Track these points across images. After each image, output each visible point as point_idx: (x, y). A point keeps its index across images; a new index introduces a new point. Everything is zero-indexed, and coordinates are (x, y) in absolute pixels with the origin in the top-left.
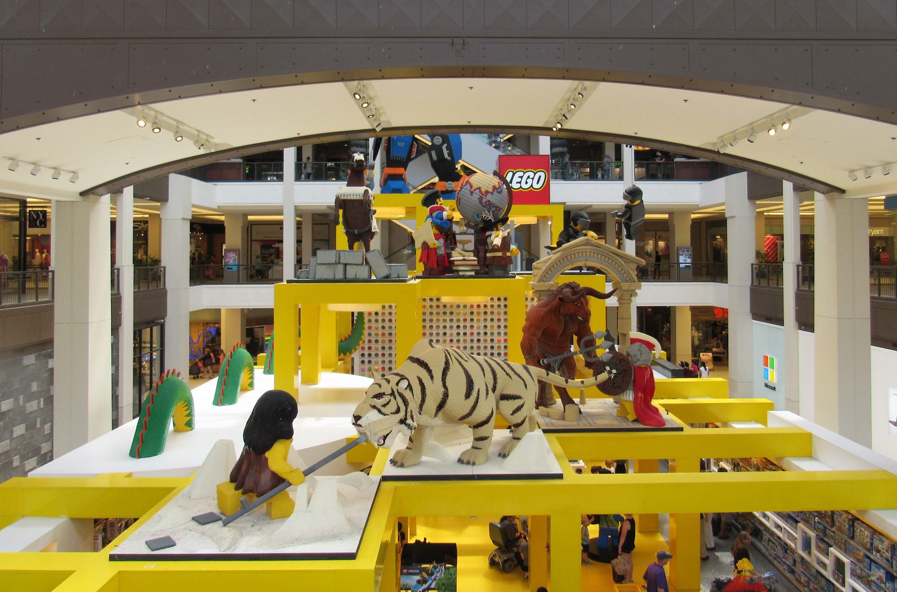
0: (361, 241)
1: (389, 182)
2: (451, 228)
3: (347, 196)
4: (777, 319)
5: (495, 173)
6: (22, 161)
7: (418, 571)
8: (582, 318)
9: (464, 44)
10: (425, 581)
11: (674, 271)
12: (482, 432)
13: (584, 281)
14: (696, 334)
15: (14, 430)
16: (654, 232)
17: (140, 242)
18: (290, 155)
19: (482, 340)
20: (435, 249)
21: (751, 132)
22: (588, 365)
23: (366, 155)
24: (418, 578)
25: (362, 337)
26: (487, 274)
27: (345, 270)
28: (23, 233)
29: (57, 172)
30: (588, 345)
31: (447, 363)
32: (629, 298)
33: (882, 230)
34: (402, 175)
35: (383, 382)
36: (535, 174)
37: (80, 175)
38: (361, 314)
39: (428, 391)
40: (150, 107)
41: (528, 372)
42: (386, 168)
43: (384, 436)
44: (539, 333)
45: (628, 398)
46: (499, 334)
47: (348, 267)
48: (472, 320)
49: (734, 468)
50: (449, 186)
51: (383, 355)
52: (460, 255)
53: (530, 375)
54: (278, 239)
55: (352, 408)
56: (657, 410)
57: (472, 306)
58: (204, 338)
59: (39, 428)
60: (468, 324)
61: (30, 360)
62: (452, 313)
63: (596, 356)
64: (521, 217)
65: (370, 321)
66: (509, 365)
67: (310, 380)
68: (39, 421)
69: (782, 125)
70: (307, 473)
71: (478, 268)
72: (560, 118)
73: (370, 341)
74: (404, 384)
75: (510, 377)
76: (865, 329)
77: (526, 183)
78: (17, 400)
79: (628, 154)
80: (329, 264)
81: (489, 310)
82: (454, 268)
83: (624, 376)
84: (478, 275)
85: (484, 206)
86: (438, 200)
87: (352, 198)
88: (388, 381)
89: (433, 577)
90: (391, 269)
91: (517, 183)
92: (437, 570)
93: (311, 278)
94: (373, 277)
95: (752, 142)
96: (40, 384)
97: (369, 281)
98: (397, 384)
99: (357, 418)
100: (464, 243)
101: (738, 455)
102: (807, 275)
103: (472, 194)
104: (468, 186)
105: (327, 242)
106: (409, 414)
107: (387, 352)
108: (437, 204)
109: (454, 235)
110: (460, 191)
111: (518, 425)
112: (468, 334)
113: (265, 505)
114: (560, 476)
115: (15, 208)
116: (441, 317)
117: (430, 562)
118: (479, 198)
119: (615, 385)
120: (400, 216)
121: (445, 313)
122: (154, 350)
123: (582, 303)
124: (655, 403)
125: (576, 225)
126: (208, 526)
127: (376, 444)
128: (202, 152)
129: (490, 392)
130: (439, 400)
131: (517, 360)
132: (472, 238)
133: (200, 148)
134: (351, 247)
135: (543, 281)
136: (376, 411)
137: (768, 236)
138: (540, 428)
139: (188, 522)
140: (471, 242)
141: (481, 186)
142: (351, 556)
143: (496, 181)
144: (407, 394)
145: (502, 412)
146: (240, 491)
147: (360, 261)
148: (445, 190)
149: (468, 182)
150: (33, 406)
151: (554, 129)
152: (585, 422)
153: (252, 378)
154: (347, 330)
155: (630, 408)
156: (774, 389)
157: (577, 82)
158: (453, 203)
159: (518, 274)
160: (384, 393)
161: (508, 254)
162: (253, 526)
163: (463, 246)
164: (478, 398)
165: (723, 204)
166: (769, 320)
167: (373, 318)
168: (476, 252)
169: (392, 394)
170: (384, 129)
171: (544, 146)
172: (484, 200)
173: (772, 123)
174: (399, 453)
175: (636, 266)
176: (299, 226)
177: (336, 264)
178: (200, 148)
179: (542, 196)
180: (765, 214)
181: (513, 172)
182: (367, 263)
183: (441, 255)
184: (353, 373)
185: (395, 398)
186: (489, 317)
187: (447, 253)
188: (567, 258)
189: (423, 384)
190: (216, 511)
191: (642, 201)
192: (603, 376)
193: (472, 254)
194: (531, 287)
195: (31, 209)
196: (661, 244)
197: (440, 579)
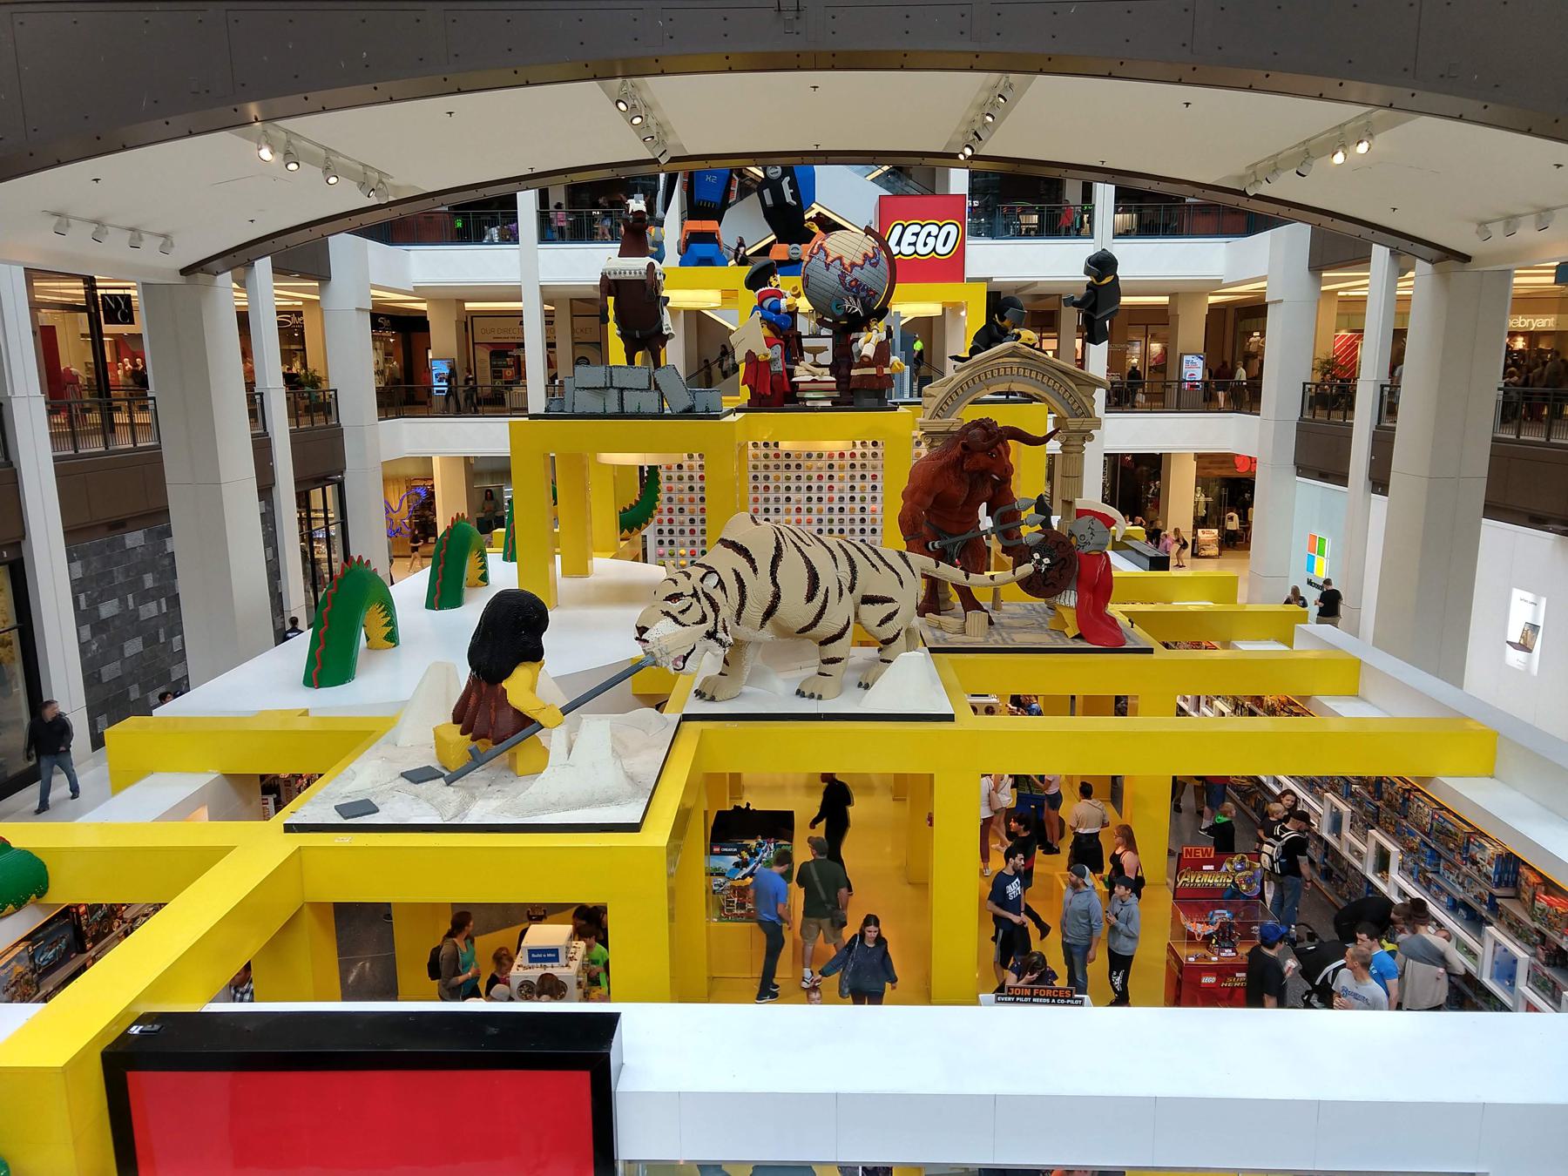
0: (646, 349)
1: (692, 245)
2: (794, 325)
3: (620, 273)
4: (1336, 474)
5: (868, 231)
6: (75, 218)
7: (735, 850)
9: (798, 10)
10: (745, 864)
11: (1172, 395)
12: (833, 650)
13: (1004, 416)
14: (1202, 499)
15: (125, 646)
16: (1144, 327)
17: (293, 347)
18: (527, 203)
20: (768, 363)
21: (1305, 155)
22: (1006, 550)
23: (651, 206)
24: (736, 859)
25: (657, 503)
26: (851, 403)
27: (621, 399)
28: (96, 335)
29: (136, 236)
30: (1007, 519)
31: (778, 548)
32: (1080, 443)
33: (1553, 319)
34: (714, 234)
35: (681, 578)
36: (940, 228)
37: (175, 240)
38: (654, 470)
40: (275, 125)
41: (906, 562)
42: (686, 222)
43: (684, 656)
44: (930, 501)
48: (831, 477)
51: (692, 532)
52: (807, 373)
53: (909, 566)
54: (516, 341)
55: (634, 614)
56: (1114, 620)
58: (408, 502)
59: (164, 643)
60: (825, 484)
61: (134, 538)
62: (798, 466)
63: (1020, 536)
64: (910, 305)
65: (669, 478)
66: (876, 552)
67: (578, 568)
68: (162, 631)
69: (1358, 144)
70: (566, 711)
71: (836, 394)
72: (971, 138)
73: (670, 510)
74: (712, 580)
75: (878, 570)
76: (1478, 493)
77: (925, 244)
78: (123, 601)
79: (1104, 194)
80: (596, 388)
81: (858, 461)
82: (798, 395)
83: (1062, 568)
84: (838, 405)
85: (846, 289)
86: (772, 279)
88: (688, 576)
89: (758, 858)
90: (694, 397)
91: (910, 244)
92: (764, 848)
93: (568, 410)
94: (667, 412)
95: (1304, 176)
96: (158, 576)
97: (660, 416)
98: (702, 580)
99: (642, 630)
100: (815, 351)
102: (1388, 405)
103: (828, 270)
104: (822, 254)
105: (591, 350)
106: (720, 625)
107: (698, 527)
108: (771, 286)
109: (799, 337)
110: (808, 263)
111: (887, 642)
112: (825, 499)
113: (506, 754)
114: (949, 718)
115: (76, 291)
116: (783, 474)
117: (753, 837)
119: (1047, 583)
120: (713, 305)
121: (788, 466)
122: (330, 522)
123: (1000, 453)
124: (1114, 609)
125: (1002, 319)
126: (424, 786)
127: (671, 667)
128: (373, 201)
129: (846, 591)
130: (767, 604)
131: (892, 541)
132: (829, 343)
133: (369, 196)
134: (631, 361)
135: (939, 416)
136: (670, 620)
137: (1342, 333)
138: (925, 646)
139: (395, 779)
141: (843, 253)
142: (634, 828)
143: (869, 244)
144: (718, 595)
145: (864, 622)
146: (469, 736)
147: (646, 385)
149: (821, 247)
150: (150, 610)
151: (961, 157)
152: (996, 637)
153: (484, 567)
154: (633, 493)
155: (1070, 617)
157: (996, 75)
158: (797, 281)
159: (902, 404)
161: (887, 371)
162: (490, 785)
163: (815, 357)
164: (826, 601)
166: (1323, 476)
167: (675, 474)
168: (834, 369)
169: (695, 595)
170: (673, 160)
171: (959, 181)
173: (1341, 139)
174: (708, 681)
176: (549, 320)
177: (606, 388)
178: (369, 196)
179: (951, 268)
180: (1340, 294)
181: (903, 225)
182: (657, 388)
183: (777, 373)
184: (645, 561)
185: (699, 601)
186: (858, 473)
188: (979, 378)
189: (742, 580)
190: (435, 764)
191: (1116, 277)
192: (1027, 569)
193: (827, 371)
194: (918, 426)
195: (103, 292)
196: (1156, 347)
197: (767, 861)
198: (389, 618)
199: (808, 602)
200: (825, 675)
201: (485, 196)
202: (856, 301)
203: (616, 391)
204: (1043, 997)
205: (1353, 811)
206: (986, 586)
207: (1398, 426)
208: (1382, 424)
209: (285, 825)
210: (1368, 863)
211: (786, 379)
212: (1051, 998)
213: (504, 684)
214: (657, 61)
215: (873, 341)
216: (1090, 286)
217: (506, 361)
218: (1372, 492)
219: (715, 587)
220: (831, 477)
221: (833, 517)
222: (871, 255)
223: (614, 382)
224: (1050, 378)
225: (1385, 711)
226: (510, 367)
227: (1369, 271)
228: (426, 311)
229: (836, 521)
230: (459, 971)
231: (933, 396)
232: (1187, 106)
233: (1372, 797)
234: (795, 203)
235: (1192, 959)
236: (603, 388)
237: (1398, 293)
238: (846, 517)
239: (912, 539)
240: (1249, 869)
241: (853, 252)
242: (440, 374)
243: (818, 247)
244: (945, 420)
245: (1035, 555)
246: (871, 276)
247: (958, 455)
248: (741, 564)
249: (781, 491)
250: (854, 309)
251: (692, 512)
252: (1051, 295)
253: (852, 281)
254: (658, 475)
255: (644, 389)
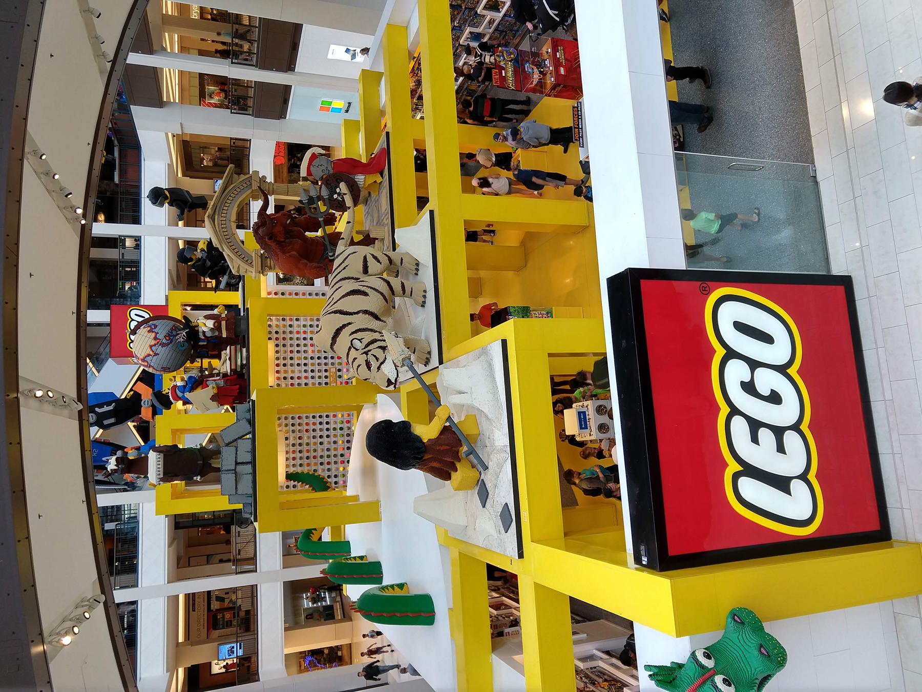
3: (159, 471)
8: (288, 220)
19: (313, 368)
20: (219, 388)
26: (244, 337)
27: (243, 463)
31: (336, 312)
39: (364, 327)
45: (362, 180)
46: (305, 352)
47: (239, 461)
48: (292, 378)
49: (419, 110)
50: (146, 403)
51: (329, 463)
52: (225, 365)
57: (278, 379)
75: (347, 266)
80: (236, 480)
82: (239, 370)
85: (171, 342)
86: (164, 393)
87: (161, 466)
93: (251, 500)
98: (357, 350)
101: (408, 102)
104: (148, 359)
108: (169, 393)
110: (154, 368)
118: (162, 347)
135: (251, 263)
140: (210, 361)
144: (365, 342)
148: (151, 408)
156: (350, 104)
160: (366, 361)
165: (167, 135)
166: (286, 101)
169: (366, 353)
172: (164, 341)
175: (235, 176)
177: (236, 473)
183: (225, 383)
186: (289, 362)
187: (223, 377)
189: (356, 330)
191: (166, 189)
198: (389, 587)
199: (368, 295)
200: (412, 291)
201: (97, 177)
202: (179, 334)
203: (238, 467)
204: (579, 123)
205: (469, 26)
206: (354, 212)
207: (254, 80)
208: (255, 64)
209: (519, 558)
210: (497, 15)
211: (229, 377)
212: (579, 118)
213: (425, 441)
214: (6, 303)
215: (204, 321)
216: (171, 204)
217: (219, 619)
218: (294, 71)
219: (361, 343)
220: (292, 378)
221: (317, 376)
222: (149, 328)
223: (232, 469)
224: (228, 199)
225: (415, 7)
226: (224, 615)
227: (163, 68)
228: (185, 668)
229: (320, 374)
230: (596, 477)
231: (239, 266)
232: (53, 56)
233: (461, 11)
234: (114, 404)
235: (552, 79)
236: (236, 475)
237: (177, 101)
238: (317, 368)
239: (328, 269)
240: (503, 53)
241: (147, 338)
242: (229, 653)
243: (144, 362)
244: (254, 259)
245: (335, 198)
246: (163, 328)
247: (275, 244)
248: (345, 336)
249: (302, 422)
250: (184, 335)
251: (316, 464)
252: (177, 266)
253: (166, 339)
254: (292, 474)
255: (236, 449)
